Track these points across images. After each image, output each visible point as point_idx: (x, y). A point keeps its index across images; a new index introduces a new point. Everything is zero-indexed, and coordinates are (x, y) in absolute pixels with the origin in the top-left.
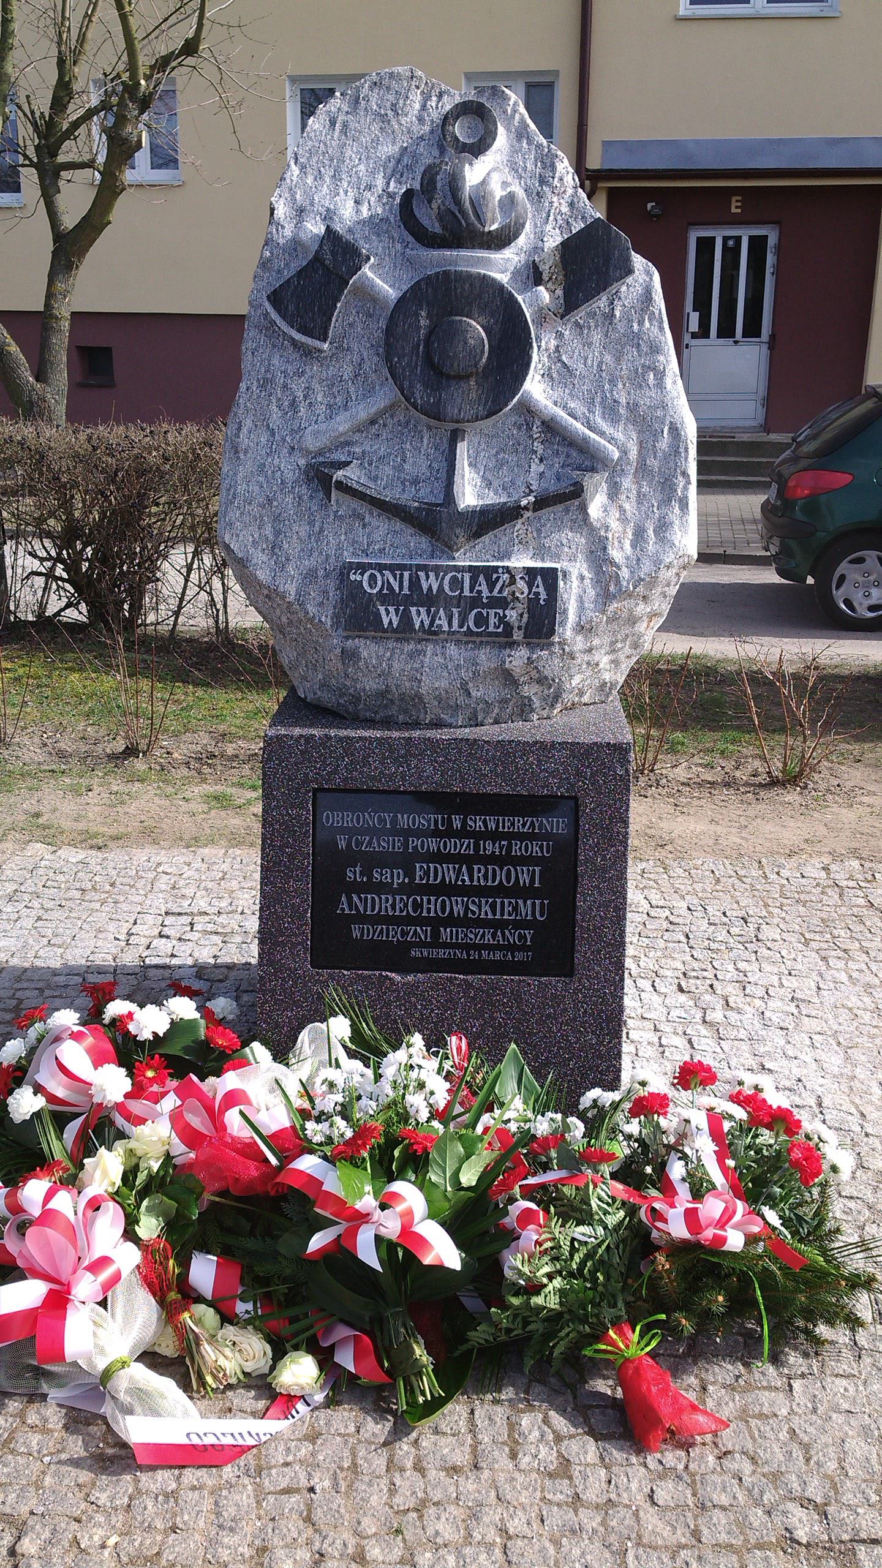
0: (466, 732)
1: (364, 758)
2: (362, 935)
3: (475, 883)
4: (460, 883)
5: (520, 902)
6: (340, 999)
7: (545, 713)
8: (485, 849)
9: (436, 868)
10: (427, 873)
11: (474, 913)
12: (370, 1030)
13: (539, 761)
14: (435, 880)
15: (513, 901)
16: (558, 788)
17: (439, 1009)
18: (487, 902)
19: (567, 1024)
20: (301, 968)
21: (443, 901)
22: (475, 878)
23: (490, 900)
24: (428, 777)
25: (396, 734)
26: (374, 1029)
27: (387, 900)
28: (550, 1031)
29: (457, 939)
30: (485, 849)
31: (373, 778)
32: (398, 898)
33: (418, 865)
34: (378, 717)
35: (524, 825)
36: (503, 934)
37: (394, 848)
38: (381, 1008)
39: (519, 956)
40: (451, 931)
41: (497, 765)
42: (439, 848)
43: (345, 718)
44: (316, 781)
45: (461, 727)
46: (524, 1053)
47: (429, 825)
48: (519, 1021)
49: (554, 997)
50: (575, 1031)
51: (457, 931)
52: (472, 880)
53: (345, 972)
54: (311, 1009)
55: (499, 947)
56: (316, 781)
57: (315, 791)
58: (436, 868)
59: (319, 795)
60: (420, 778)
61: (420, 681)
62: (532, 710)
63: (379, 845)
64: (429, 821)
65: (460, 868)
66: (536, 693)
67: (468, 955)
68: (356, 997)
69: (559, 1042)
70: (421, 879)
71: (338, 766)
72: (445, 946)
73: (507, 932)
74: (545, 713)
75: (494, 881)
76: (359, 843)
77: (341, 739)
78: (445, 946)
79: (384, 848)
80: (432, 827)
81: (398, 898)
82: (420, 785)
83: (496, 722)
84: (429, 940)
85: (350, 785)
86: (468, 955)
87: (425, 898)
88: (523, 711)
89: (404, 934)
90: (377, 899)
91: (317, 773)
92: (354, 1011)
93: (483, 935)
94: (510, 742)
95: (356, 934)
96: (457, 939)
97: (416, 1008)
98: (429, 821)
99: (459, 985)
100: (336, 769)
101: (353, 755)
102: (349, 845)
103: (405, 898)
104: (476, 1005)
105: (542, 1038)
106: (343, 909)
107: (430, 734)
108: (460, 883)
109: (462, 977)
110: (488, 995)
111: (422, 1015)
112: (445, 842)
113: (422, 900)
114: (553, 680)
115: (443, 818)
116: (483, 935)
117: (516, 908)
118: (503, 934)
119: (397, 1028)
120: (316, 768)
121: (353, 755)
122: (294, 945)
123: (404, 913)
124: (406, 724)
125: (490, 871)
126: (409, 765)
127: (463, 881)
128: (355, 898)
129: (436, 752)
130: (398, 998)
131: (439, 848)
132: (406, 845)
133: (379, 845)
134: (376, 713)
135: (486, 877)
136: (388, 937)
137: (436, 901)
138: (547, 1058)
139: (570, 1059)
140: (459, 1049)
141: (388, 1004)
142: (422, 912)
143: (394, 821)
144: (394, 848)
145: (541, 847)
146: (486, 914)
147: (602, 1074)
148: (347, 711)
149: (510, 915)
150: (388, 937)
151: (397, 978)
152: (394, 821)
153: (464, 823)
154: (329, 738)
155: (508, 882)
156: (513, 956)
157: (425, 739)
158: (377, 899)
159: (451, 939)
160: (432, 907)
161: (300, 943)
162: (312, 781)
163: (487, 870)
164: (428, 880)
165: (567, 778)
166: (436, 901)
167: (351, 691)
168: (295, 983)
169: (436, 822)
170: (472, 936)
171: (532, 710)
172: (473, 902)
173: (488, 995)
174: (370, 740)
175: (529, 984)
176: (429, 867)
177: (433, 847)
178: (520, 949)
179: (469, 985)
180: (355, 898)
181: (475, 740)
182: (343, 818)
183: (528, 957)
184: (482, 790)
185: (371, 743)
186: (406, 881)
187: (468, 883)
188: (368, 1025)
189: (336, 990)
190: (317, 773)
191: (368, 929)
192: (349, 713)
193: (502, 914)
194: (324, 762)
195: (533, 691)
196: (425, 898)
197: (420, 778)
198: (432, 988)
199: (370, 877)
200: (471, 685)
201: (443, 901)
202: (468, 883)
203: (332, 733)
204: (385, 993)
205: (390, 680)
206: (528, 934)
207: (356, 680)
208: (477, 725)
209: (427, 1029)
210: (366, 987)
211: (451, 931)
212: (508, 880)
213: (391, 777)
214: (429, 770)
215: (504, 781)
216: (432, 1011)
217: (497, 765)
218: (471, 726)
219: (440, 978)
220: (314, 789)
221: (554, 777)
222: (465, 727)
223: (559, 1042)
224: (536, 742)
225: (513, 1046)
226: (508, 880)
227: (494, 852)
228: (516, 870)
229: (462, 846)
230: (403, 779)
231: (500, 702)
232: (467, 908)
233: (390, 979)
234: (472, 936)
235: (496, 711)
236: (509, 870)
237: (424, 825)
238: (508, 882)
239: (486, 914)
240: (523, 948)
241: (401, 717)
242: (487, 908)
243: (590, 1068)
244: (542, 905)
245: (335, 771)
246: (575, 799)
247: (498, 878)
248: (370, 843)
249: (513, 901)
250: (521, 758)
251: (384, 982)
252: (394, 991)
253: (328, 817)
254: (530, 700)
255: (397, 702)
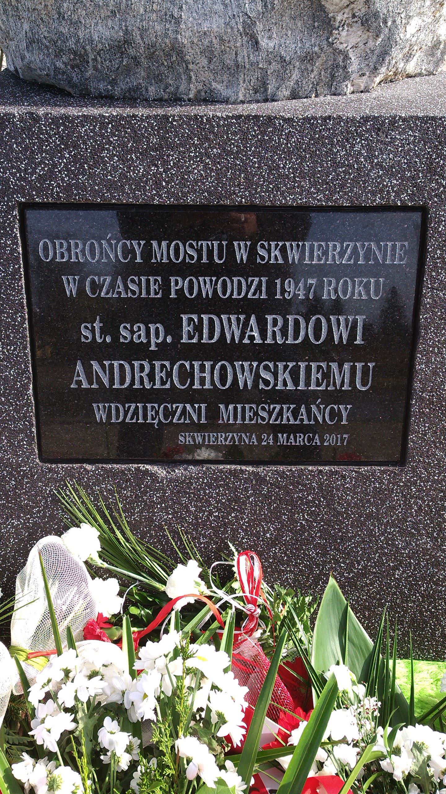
0: (253, 109)
1: (95, 152)
2: (109, 416)
3: (269, 341)
4: (246, 341)
5: (334, 366)
6: (83, 503)
7: (362, 83)
8: (283, 291)
9: (211, 321)
10: (199, 328)
11: (267, 383)
12: (127, 540)
13: (370, 149)
14: (211, 337)
15: (324, 365)
16: (398, 194)
17: (219, 510)
18: (286, 367)
19: (393, 525)
20: (26, 463)
21: (223, 368)
22: (269, 333)
23: (291, 365)
24: (196, 181)
25: (141, 112)
26: (132, 538)
27: (142, 368)
28: (371, 534)
29: (243, 418)
30: (283, 291)
31: (110, 186)
32: (157, 364)
33: (185, 317)
34: (117, 92)
35: (342, 254)
36: (309, 411)
37: (148, 292)
38: (141, 512)
39: (330, 440)
40: (235, 409)
41: (303, 159)
42: (215, 291)
43: (69, 95)
44: (21, 190)
45: (243, 102)
46: (342, 587)
47: (200, 257)
48: (328, 523)
49: (377, 492)
50: (402, 532)
51: (243, 409)
52: (296, 442)
53: (89, 467)
54: (44, 516)
55: (301, 429)
56: (21, 190)
57: (24, 208)
58: (211, 321)
59: (30, 214)
60: (183, 183)
61: (178, 21)
62: (346, 77)
63: (126, 288)
64: (199, 251)
65: (247, 320)
66: (355, 47)
67: (260, 440)
68: (106, 499)
69: (382, 548)
70: (191, 337)
71: (55, 166)
72: (227, 428)
73: (314, 408)
74: (362, 83)
75: (296, 337)
76: (95, 287)
77: (55, 120)
78: (227, 428)
79: (133, 292)
80: (205, 260)
81: (157, 364)
82: (185, 195)
83: (294, 96)
84: (203, 421)
85: (77, 197)
86: (260, 440)
87: (196, 364)
88: (333, 77)
89: (168, 414)
90: (127, 367)
91: (21, 179)
92: (103, 516)
93: (281, 413)
94: (325, 119)
95: (100, 415)
96: (243, 418)
97: (188, 511)
98: (199, 251)
99: (246, 480)
100: (51, 171)
101: (76, 146)
102: (81, 290)
103: (167, 364)
104: (270, 504)
105: (358, 544)
106: (79, 383)
107: (194, 110)
108: (246, 341)
109: (250, 469)
110: (287, 493)
111: (196, 519)
112: (224, 282)
113: (192, 366)
114: (385, 22)
115: (220, 246)
116: (281, 413)
117: (327, 375)
118: (309, 411)
119: (164, 536)
120: (19, 170)
121: (76, 146)
122: (14, 433)
123: (168, 386)
124: (161, 100)
125: (291, 323)
126: (165, 163)
127: (252, 338)
128: (95, 366)
129: (207, 139)
130: (163, 499)
131: (215, 291)
132: (166, 287)
133: (126, 288)
134: (113, 83)
135: (284, 332)
136: (145, 417)
137: (213, 368)
138: (365, 567)
139: (395, 568)
140: (250, 575)
141: (151, 506)
142: (192, 383)
143: (147, 253)
144: (148, 292)
145: (367, 287)
146: (285, 384)
147: (436, 584)
148: (70, 81)
149: (318, 385)
150: (145, 417)
151: (160, 471)
152: (147, 253)
153: (252, 253)
154: (36, 119)
155: (317, 337)
156: (322, 440)
157: (189, 118)
158: (127, 367)
159: (235, 418)
160: (207, 375)
161: (21, 431)
162: (15, 192)
163: (286, 321)
164: (201, 337)
165: (413, 178)
166: (213, 368)
167: (71, 43)
168: (20, 483)
169: (210, 253)
170: (265, 415)
171: (346, 77)
172: (266, 368)
173: (287, 493)
174: (101, 121)
175: (344, 477)
176: (201, 320)
177: (207, 290)
178: (331, 430)
179: (261, 480)
180: (95, 366)
181: (269, 117)
182: (69, 249)
183: (342, 440)
184: (280, 201)
185: (104, 126)
186: (169, 339)
187: (258, 340)
188: (123, 533)
189: (76, 491)
190: (21, 179)
191: (117, 409)
192: (74, 86)
193: (308, 384)
194: (31, 159)
195: (353, 41)
196: (196, 364)
197: (183, 183)
198: (210, 485)
199: (116, 336)
200: (259, 26)
201: (223, 368)
202: (258, 340)
203: (41, 111)
204: (145, 493)
205: (130, 20)
206: (344, 410)
207: (76, 24)
208: (266, 100)
209: (204, 536)
210: (119, 486)
211: (235, 409)
212: (317, 336)
213: (139, 183)
214: (197, 171)
215: (312, 185)
216: (211, 513)
217: (303, 159)
218: (258, 101)
219: (221, 471)
220: (20, 204)
221: (393, 175)
222: (250, 102)
223: (382, 548)
224: (366, 119)
225: (332, 581)
226: (317, 336)
227: (296, 296)
228: (329, 321)
229: (249, 287)
230: (157, 185)
231: (302, 60)
232: (257, 376)
233: (152, 475)
234: (265, 415)
235: (296, 75)
236: (318, 321)
237: (191, 257)
238: (317, 337)
239: (285, 384)
240: (337, 428)
241: (152, 89)
242: (287, 376)
243: (423, 578)
244: (365, 370)
245: (51, 175)
246: (424, 210)
247: (302, 333)
248: (113, 286)
249: (324, 365)
250: (343, 147)
251: (142, 480)
252: (157, 490)
253: (46, 248)
254: (346, 57)
255: (144, 62)
